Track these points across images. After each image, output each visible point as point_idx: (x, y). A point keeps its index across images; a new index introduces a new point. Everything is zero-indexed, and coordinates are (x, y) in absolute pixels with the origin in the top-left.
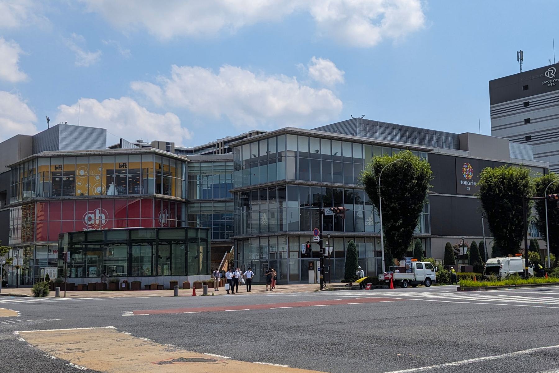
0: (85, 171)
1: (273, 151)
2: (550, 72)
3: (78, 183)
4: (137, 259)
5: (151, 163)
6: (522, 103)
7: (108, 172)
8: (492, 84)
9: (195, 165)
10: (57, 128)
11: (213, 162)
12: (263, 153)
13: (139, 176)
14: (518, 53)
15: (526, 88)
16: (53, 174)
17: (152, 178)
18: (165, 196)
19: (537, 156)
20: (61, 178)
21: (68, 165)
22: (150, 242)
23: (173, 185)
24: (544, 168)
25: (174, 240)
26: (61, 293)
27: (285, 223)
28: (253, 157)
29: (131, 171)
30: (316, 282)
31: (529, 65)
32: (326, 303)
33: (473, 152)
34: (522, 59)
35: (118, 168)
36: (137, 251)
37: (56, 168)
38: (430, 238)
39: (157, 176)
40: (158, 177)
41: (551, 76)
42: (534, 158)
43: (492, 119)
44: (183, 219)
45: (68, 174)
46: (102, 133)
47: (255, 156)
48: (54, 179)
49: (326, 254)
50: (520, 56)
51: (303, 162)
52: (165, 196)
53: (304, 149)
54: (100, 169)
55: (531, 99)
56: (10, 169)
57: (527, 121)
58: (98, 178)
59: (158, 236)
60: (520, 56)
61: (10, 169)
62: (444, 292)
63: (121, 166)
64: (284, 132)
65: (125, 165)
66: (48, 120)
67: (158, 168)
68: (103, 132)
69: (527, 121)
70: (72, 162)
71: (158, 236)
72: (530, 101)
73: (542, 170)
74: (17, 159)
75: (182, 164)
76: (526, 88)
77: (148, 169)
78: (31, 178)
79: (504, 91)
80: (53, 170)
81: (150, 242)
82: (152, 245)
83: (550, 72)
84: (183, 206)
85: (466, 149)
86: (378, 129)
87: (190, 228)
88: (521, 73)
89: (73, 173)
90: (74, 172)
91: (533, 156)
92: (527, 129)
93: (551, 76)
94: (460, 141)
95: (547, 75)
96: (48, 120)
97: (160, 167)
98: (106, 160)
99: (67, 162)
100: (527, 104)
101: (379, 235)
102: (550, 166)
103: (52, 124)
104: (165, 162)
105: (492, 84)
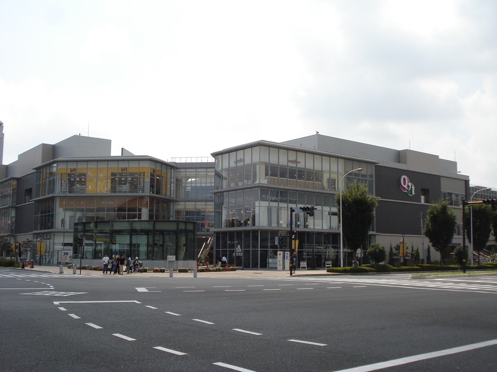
4: (135, 245)
7: (113, 174)
8: (109, 141)
9: (182, 170)
13: (137, 178)
16: (69, 175)
17: (148, 180)
18: (158, 196)
20: (75, 179)
21: (81, 167)
22: (146, 232)
23: (164, 186)
25: (166, 231)
26: (78, 271)
29: (131, 174)
30: (284, 269)
32: (309, 286)
35: (120, 171)
36: (136, 240)
37: (71, 170)
38: (375, 235)
39: (151, 178)
40: (152, 180)
44: (171, 215)
45: (80, 175)
46: (107, 143)
48: (69, 180)
52: (158, 196)
53: (274, 160)
56: (35, 171)
59: (154, 227)
61: (35, 171)
62: (399, 279)
63: (122, 170)
65: (126, 169)
67: (152, 172)
68: (107, 143)
73: (464, 182)
74: (40, 164)
75: (171, 169)
78: (51, 179)
80: (69, 172)
81: (146, 232)
82: (148, 235)
84: (172, 204)
85: (405, 163)
89: (85, 175)
97: (154, 171)
98: (113, 165)
101: (337, 231)
104: (158, 168)
105: (109, 141)
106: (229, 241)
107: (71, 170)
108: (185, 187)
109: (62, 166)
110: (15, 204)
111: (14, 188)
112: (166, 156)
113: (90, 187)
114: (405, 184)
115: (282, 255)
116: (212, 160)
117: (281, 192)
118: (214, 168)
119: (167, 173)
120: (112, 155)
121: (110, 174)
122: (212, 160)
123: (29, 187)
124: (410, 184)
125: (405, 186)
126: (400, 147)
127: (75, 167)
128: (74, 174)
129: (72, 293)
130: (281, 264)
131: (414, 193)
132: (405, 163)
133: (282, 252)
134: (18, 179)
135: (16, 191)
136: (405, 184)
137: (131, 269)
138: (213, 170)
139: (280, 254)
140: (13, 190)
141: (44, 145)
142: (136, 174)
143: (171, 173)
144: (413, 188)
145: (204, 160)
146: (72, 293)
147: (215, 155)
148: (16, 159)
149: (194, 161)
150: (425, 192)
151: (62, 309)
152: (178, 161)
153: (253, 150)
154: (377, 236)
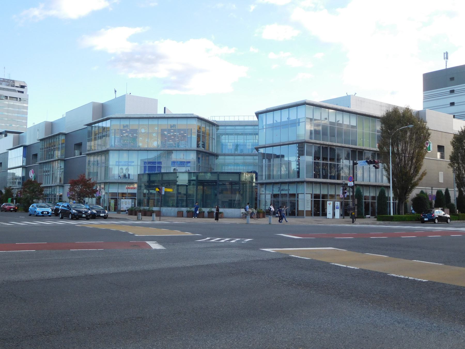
0: (145, 130)
3: (140, 138)
5: (195, 124)
6: (449, 90)
10: (123, 97)
11: (236, 126)
12: (285, 119)
14: (444, 53)
15: (452, 79)
27: (291, 172)
28: (275, 122)
29: (179, 130)
31: (453, 63)
34: (447, 58)
35: (169, 128)
37: (124, 127)
40: (198, 136)
43: (424, 102)
46: (155, 102)
47: (276, 121)
50: (446, 56)
54: (156, 128)
57: (452, 104)
58: (154, 135)
59: (218, 178)
60: (446, 56)
64: (304, 104)
66: (116, 91)
68: (155, 102)
69: (452, 104)
70: (136, 122)
71: (218, 178)
72: (455, 89)
74: (91, 121)
76: (452, 79)
77: (191, 129)
79: (433, 81)
80: (122, 128)
87: (153, 174)
90: (137, 130)
96: (116, 91)
99: (133, 122)
100: (452, 92)
103: (118, 95)
107: (124, 127)
109: (116, 122)
110: (64, 157)
111: (62, 142)
115: (331, 205)
117: (330, 148)
119: (209, 130)
120: (158, 113)
123: (78, 142)
130: (331, 212)
133: (332, 202)
134: (65, 134)
135: (64, 145)
137: (33, 191)
139: (330, 204)
141: (94, 103)
143: (213, 129)
147: (258, 114)
151: (155, 246)
152: (217, 119)
153: (282, 113)
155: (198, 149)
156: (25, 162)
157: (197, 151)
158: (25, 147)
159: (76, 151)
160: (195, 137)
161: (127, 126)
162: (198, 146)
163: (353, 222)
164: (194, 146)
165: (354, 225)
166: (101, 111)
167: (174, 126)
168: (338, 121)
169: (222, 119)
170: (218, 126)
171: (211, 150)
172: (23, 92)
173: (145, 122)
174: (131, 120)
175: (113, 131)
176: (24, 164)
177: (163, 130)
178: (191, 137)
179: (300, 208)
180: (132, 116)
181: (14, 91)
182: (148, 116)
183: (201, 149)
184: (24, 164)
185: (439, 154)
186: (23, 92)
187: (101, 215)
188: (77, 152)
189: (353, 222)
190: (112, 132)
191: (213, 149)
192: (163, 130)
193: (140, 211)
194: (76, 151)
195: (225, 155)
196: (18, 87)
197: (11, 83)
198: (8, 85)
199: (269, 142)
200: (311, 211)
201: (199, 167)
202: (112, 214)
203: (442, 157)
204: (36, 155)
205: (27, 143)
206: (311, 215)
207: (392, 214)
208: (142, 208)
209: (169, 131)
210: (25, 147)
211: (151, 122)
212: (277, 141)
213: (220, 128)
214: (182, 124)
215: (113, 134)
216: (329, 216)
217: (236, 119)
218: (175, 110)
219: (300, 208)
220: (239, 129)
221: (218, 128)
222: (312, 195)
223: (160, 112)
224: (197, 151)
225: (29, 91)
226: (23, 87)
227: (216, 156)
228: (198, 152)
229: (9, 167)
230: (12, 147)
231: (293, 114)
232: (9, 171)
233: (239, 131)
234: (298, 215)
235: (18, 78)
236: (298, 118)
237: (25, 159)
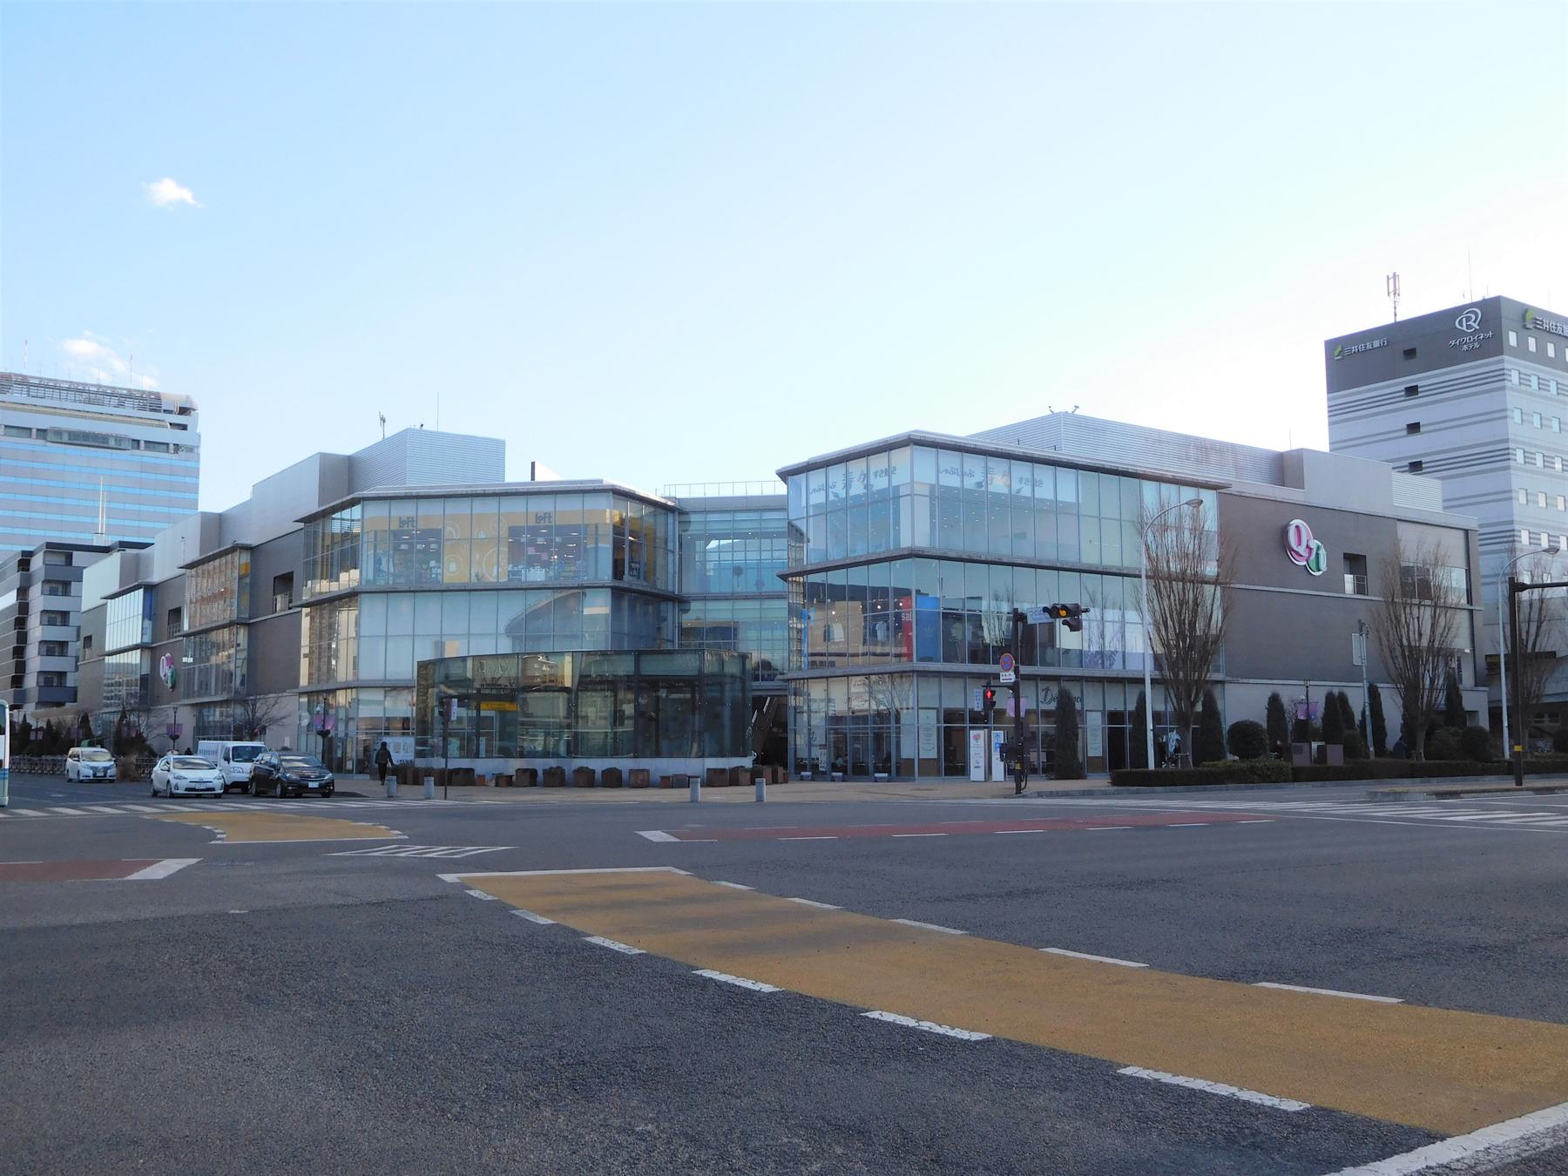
1: (879, 483)
2: (1468, 319)
8: (503, 443)
12: (857, 489)
19: (1450, 503)
20: (412, 546)
21: (429, 513)
24: (1466, 531)
31: (1414, 306)
33: (1315, 492)
35: (532, 523)
37: (402, 522)
38: (1222, 682)
39: (852, 599)
40: (618, 546)
41: (1469, 327)
42: (1445, 508)
43: (1331, 424)
47: (836, 495)
49: (1171, 749)
51: (944, 501)
55: (1421, 379)
57: (1414, 428)
61: (302, 525)
68: (494, 450)
69: (1414, 428)
71: (524, 670)
72: (1419, 384)
73: (1461, 534)
74: (314, 507)
76: (1410, 353)
80: (395, 526)
82: (615, 692)
83: (1468, 319)
85: (1299, 484)
86: (822, 757)
88: (1396, 323)
91: (1440, 504)
92: (1414, 446)
93: (1469, 327)
94: (1285, 468)
95: (1461, 323)
98: (508, 506)
100: (1412, 391)
102: (1481, 526)
103: (392, 430)
105: (503, 443)
106: (1221, 756)
107: (402, 522)
108: (704, 563)
109: (376, 511)
112: (656, 482)
113: (453, 567)
114: (1299, 544)
115: (981, 741)
116: (781, 488)
118: (784, 509)
120: (508, 479)
121: (504, 533)
122: (781, 488)
124: (1314, 543)
125: (1302, 550)
126: (1282, 446)
127: (413, 514)
128: (408, 533)
129: (471, 850)
130: (982, 764)
131: (1323, 566)
132: (1299, 484)
133: (981, 732)
134: (250, 549)
136: (1299, 544)
138: (781, 515)
139: (976, 738)
140: (240, 578)
142: (576, 528)
144: (1323, 552)
145: (754, 491)
146: (471, 850)
147: (785, 475)
148: (245, 495)
149: (726, 492)
150: (1355, 562)
152: (682, 493)
154: (1227, 686)
155: (617, 584)
156: (149, 631)
157: (613, 589)
158: (150, 589)
159: (279, 598)
160: (606, 546)
161: (410, 520)
162: (618, 572)
163: (1019, 790)
164: (606, 573)
165: (1021, 801)
166: (343, 479)
167: (547, 516)
168: (1019, 491)
169: (697, 493)
170: (682, 512)
171: (670, 588)
172: (184, 427)
173: (462, 507)
174: (560, 498)
175: (372, 536)
176: (147, 639)
177: (514, 532)
178: (596, 549)
179: (907, 752)
180: (422, 492)
181: (160, 424)
182: (469, 490)
183: (628, 580)
184: (147, 639)
185: (1349, 579)
186: (184, 427)
187: (311, 785)
188: (280, 601)
189: (1019, 790)
190: (367, 540)
191: (666, 582)
192: (514, 532)
193: (429, 772)
194: (279, 598)
195: (705, 598)
196: (170, 412)
197: (153, 403)
198: (142, 408)
199: (836, 555)
200: (605, 745)
201: (616, 634)
202: (362, 783)
203: (1360, 588)
204: (176, 613)
205: (156, 578)
206: (939, 774)
207: (1152, 766)
208: (438, 763)
209: (534, 531)
210: (150, 589)
211: (480, 507)
212: (861, 552)
213: (693, 518)
214: (568, 510)
215: (372, 547)
216: (977, 773)
217: (740, 491)
218: (547, 475)
219: (907, 752)
220: (746, 521)
221: (684, 518)
222: (1103, 712)
223: (515, 474)
224: (613, 589)
225: (205, 425)
226: (184, 411)
227: (681, 602)
228: (618, 593)
229: (109, 647)
230: (116, 589)
231: (878, 477)
232: (108, 660)
233: (744, 525)
234: (898, 773)
235: (173, 390)
236: (894, 484)
237: (148, 623)
